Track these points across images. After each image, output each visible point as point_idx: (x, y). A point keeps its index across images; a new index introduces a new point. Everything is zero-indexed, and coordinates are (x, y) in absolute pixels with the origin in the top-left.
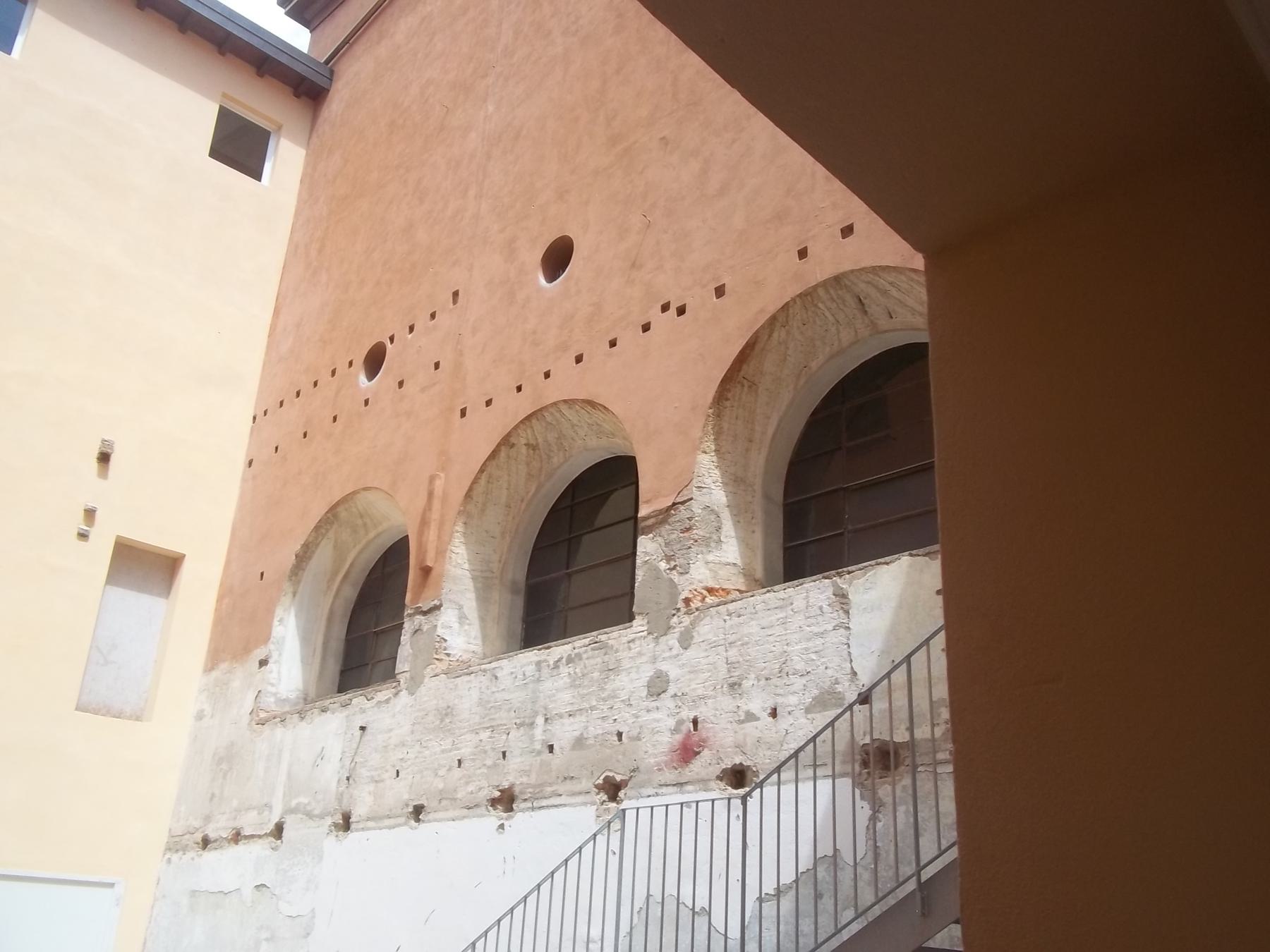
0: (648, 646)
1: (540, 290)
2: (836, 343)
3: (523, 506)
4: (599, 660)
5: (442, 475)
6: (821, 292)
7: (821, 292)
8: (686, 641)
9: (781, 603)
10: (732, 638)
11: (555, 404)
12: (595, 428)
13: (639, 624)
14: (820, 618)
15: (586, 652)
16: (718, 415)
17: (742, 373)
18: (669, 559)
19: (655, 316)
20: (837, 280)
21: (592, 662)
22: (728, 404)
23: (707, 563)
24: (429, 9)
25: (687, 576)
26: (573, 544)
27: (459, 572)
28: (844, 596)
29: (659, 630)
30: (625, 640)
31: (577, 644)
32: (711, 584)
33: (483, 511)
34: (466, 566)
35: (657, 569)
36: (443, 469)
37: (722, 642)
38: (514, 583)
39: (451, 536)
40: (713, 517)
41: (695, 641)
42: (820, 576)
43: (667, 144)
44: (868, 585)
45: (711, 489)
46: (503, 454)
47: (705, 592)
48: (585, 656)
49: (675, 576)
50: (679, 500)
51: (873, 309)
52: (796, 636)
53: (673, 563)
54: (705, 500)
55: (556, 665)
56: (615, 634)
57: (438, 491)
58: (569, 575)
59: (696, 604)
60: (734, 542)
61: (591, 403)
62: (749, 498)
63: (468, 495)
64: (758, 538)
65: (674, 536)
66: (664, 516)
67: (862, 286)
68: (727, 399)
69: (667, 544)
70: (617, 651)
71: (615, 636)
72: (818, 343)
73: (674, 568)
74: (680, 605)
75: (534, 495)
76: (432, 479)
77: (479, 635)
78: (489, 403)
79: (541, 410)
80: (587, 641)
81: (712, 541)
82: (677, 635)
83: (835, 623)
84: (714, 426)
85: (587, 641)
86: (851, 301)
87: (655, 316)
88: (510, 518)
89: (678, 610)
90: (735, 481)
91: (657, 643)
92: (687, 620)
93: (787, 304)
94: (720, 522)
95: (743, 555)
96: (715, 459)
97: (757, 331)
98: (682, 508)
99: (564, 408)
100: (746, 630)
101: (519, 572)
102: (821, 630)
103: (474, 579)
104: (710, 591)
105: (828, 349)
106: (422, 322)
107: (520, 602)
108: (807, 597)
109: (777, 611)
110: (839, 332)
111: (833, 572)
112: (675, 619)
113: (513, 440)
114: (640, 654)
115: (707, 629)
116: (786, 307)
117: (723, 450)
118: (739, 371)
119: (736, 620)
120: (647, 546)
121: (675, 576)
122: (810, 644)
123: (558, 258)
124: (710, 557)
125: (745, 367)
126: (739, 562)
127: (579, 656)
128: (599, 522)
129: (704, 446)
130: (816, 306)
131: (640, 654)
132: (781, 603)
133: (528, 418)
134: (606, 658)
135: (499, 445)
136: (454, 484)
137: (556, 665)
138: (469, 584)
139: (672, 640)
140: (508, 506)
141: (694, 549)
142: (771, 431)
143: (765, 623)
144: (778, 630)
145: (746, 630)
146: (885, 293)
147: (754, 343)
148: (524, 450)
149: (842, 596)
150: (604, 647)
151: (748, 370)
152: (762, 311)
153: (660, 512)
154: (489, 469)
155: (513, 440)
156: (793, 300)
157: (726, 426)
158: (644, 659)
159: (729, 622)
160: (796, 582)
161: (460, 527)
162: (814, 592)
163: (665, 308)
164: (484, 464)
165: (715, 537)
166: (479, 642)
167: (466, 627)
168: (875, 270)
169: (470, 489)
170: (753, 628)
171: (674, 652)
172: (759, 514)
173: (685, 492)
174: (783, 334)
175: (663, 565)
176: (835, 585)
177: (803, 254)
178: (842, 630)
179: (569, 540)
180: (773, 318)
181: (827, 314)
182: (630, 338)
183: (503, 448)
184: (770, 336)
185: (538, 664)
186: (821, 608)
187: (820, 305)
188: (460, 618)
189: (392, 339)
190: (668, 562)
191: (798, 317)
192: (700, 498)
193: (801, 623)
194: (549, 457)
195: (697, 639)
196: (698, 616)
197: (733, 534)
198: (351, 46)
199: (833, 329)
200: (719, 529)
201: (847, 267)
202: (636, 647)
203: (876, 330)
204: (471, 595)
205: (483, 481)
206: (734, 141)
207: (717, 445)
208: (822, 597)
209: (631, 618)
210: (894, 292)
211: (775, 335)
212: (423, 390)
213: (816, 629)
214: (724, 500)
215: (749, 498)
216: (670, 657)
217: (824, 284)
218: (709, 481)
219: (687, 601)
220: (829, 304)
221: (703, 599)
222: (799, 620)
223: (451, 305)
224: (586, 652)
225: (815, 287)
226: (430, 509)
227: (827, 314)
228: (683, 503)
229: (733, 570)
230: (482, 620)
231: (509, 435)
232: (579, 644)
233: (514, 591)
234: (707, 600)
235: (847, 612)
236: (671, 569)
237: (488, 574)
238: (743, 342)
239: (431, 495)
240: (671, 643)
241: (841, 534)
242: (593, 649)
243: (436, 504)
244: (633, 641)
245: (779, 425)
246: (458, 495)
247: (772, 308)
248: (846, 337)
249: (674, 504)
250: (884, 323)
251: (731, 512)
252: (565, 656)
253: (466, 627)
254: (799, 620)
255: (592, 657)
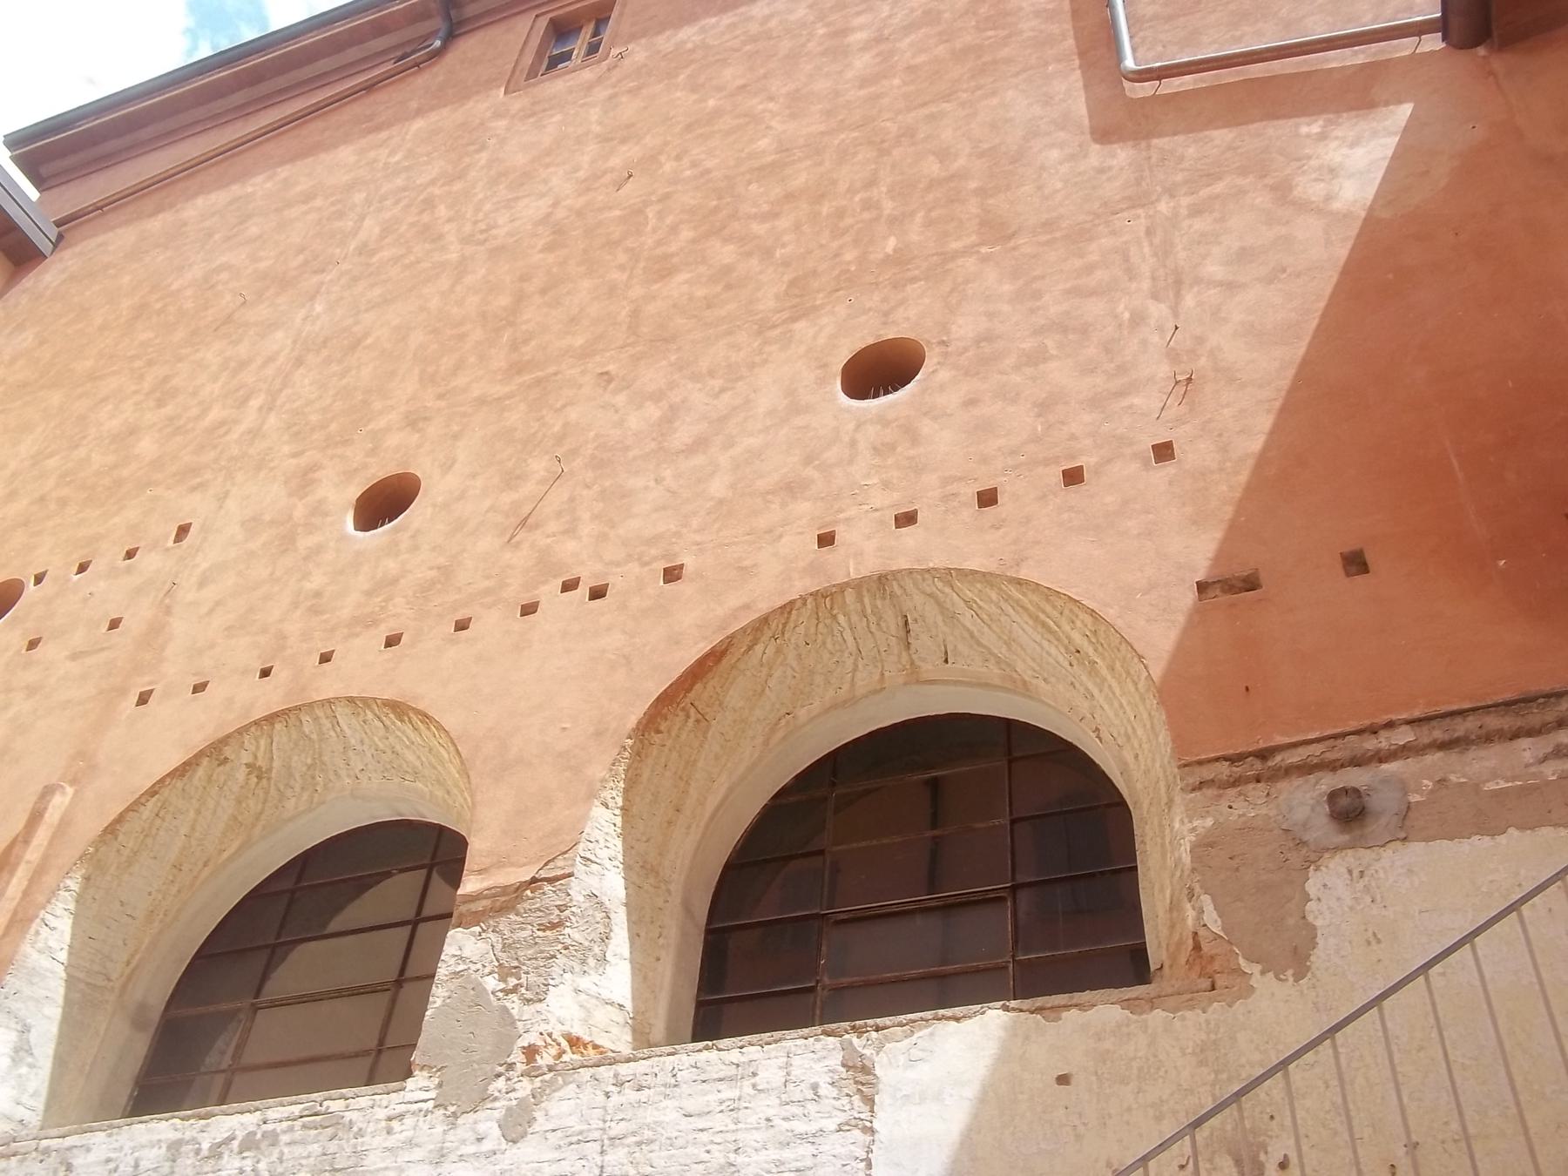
0: (432, 1129)
1: (344, 538)
2: (846, 687)
3: (206, 872)
4: (316, 1148)
5: (70, 790)
6: (850, 596)
7: (850, 596)
8: (516, 1126)
9: (732, 1071)
10: (617, 1129)
11: (329, 701)
12: (388, 756)
13: (419, 1085)
14: (811, 1107)
15: (291, 1129)
16: (638, 754)
17: (692, 695)
18: (504, 973)
19: (549, 592)
20: (882, 581)
21: (299, 1150)
22: (656, 738)
23: (578, 991)
24: (250, 190)
25: (538, 1006)
26: (276, 953)
27: (45, 962)
28: (866, 1070)
29: (460, 1099)
30: (381, 1114)
31: (272, 1114)
32: (578, 1031)
33: (130, 863)
34: (63, 956)
35: (478, 989)
36: (73, 782)
37: (596, 1135)
38: (142, 1007)
39: (53, 894)
40: (599, 916)
41: (536, 1127)
42: (818, 1029)
43: (609, 381)
44: (916, 1054)
45: (602, 876)
46: (201, 772)
47: (565, 1044)
48: (285, 1138)
49: (514, 1004)
50: (543, 874)
51: (922, 641)
52: (758, 1135)
53: (512, 981)
54: (593, 883)
55: (216, 1152)
56: (364, 1102)
57: (53, 815)
58: (255, 1009)
59: (544, 1060)
60: (625, 968)
61: (398, 708)
62: (660, 902)
63: (111, 830)
64: (666, 970)
65: (526, 934)
66: (507, 900)
67: (919, 599)
68: (658, 732)
69: (506, 947)
70: (360, 1133)
71: (363, 1107)
72: (819, 679)
73: (514, 990)
74: (517, 1057)
75: (231, 859)
76: (48, 792)
77: (44, 1092)
78: (199, 688)
79: (298, 708)
80: (296, 1109)
81: (592, 956)
82: (497, 1114)
83: (842, 1118)
84: (629, 767)
85: (296, 1109)
86: (892, 623)
87: (549, 592)
88: (174, 890)
89: (511, 1066)
90: (642, 868)
91: (454, 1126)
92: (525, 1088)
93: (792, 603)
94: (608, 925)
95: (636, 996)
96: (619, 821)
97: (732, 636)
98: (547, 888)
99: (342, 712)
100: (649, 1115)
101: (157, 985)
102: (812, 1127)
103: (71, 982)
104: (574, 1042)
105: (831, 693)
106: (108, 557)
107: (141, 1046)
108: (788, 1065)
109: (722, 1086)
110: (855, 669)
111: (846, 1025)
112: (500, 1083)
113: (228, 751)
114: (411, 1143)
115: (567, 1107)
116: (787, 608)
117: (634, 810)
118: (689, 690)
119: (630, 1094)
120: (462, 948)
121: (514, 1004)
122: (787, 1154)
123: (384, 503)
124: (584, 983)
125: (698, 686)
126: (629, 1006)
127: (273, 1139)
128: (333, 926)
129: (606, 794)
130: (834, 617)
131: (411, 1143)
132: (732, 1071)
133: (271, 719)
134: (332, 1147)
135: (200, 755)
136: (83, 811)
137: (216, 1152)
138: (56, 987)
139: (487, 1122)
140: (177, 867)
141: (561, 960)
142: (713, 802)
143: (690, 1105)
144: (719, 1121)
145: (649, 1115)
146: (951, 617)
147: (724, 653)
148: (241, 774)
149: (861, 1074)
150: (335, 1124)
151: (701, 693)
152: (746, 607)
153: (505, 890)
154: (165, 792)
155: (228, 751)
156: (804, 599)
157: (646, 774)
158: (417, 1154)
159: (615, 1099)
160: (766, 1036)
161: (74, 884)
162: (797, 1061)
163: (569, 586)
164: (162, 780)
165: (597, 950)
166: (40, 1104)
167: (24, 1070)
168: (949, 575)
169: (120, 819)
170: (667, 1113)
171: (486, 1146)
172: (673, 933)
173: (560, 863)
174: (770, 651)
175: (492, 983)
176: (847, 1048)
177: (826, 540)
178: (857, 1133)
179: (274, 948)
180: (765, 620)
181: (848, 635)
182: (492, 624)
183: (205, 761)
184: (750, 648)
185: (175, 1147)
186: (815, 1087)
187: (841, 618)
188: (17, 1050)
189: (39, 579)
190: (503, 979)
191: (801, 629)
192: (583, 876)
193: (770, 1112)
194: (282, 796)
195: (541, 1124)
196: (550, 1083)
197: (627, 954)
198: (104, 214)
199: (849, 662)
200: (605, 938)
201: (902, 563)
202: (403, 1130)
203: (914, 677)
204: (55, 1012)
205: (147, 812)
206: (723, 390)
207: (625, 799)
208: (818, 1067)
209: (409, 1074)
210: (967, 618)
211: (759, 648)
212: (74, 657)
213: (800, 1127)
214: (622, 894)
215: (660, 902)
216: (476, 1155)
217: (858, 585)
218: (603, 854)
219: (531, 1052)
220: (855, 618)
221: (560, 1055)
222: (767, 1106)
223: (170, 543)
224: (291, 1129)
225: (842, 588)
226: (27, 842)
227: (848, 635)
228: (551, 880)
229: (619, 1017)
230: (60, 1062)
231: (225, 741)
232: (279, 1112)
233: (138, 1023)
234: (565, 1058)
235: (870, 1101)
236: (507, 992)
237: (100, 982)
238: (704, 647)
239: (36, 817)
240: (482, 1128)
241: (811, 990)
242: (304, 1127)
243: (42, 836)
244: (401, 1117)
245: (726, 797)
246: (90, 826)
247: (764, 607)
248: (865, 679)
249: (534, 880)
250: (930, 666)
251: (629, 914)
252: (240, 1135)
253: (24, 1070)
254: (767, 1106)
255: (303, 1142)
